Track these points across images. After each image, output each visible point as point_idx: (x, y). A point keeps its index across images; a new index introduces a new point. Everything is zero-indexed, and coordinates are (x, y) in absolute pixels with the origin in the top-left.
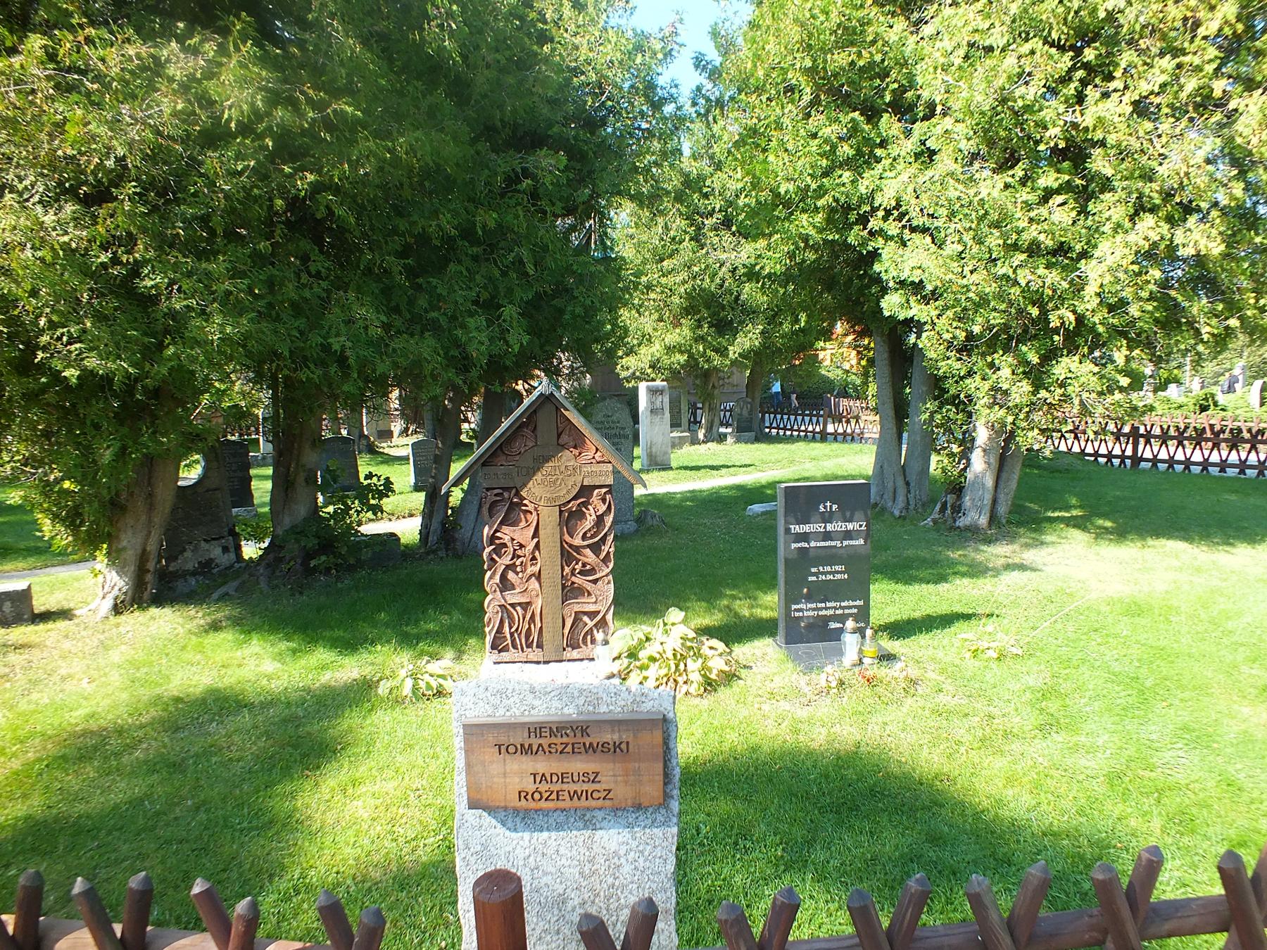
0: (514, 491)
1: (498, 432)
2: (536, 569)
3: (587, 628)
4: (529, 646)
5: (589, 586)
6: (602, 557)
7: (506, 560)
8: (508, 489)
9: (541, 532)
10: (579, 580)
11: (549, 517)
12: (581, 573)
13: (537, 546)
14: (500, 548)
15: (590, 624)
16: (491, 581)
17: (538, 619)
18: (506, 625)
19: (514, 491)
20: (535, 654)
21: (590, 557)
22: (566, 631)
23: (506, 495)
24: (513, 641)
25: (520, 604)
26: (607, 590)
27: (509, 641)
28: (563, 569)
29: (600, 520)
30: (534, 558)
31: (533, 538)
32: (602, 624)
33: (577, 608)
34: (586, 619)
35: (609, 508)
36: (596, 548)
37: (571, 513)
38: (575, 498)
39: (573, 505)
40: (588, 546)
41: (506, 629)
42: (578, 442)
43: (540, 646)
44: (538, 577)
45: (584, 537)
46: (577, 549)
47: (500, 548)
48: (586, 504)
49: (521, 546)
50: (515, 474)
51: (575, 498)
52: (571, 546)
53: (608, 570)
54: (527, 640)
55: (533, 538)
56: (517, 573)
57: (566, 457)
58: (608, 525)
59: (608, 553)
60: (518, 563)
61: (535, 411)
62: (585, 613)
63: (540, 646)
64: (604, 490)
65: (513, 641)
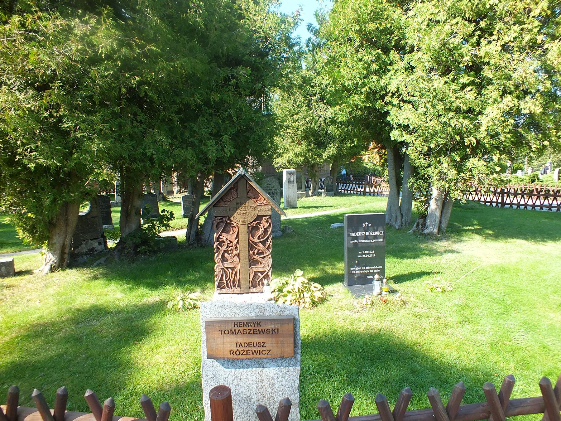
0: (227, 218)
1: (220, 192)
2: (237, 252)
3: (260, 279)
4: (234, 286)
5: (261, 260)
6: (266, 247)
7: (224, 248)
8: (225, 217)
9: (240, 236)
10: (256, 257)
11: (243, 229)
12: (257, 254)
13: (238, 242)
14: (221, 243)
15: (261, 276)
16: (217, 257)
17: (238, 274)
18: (224, 277)
19: (227, 218)
20: (237, 290)
21: (261, 247)
22: (251, 280)
23: (224, 219)
24: (227, 284)
25: (230, 268)
26: (269, 261)
27: (225, 284)
28: (249, 252)
29: (266, 230)
30: (236, 247)
31: (236, 238)
32: (267, 276)
33: (256, 269)
34: (259, 274)
35: (270, 225)
36: (264, 243)
37: (253, 227)
38: (254, 221)
39: (254, 224)
40: (260, 242)
41: (224, 279)
42: (256, 196)
43: (239, 286)
44: (238, 255)
45: (259, 238)
46: (256, 243)
47: (221, 243)
48: (259, 223)
49: (231, 242)
50: (228, 210)
51: (254, 221)
52: (253, 242)
53: (269, 253)
54: (233, 284)
55: (236, 238)
56: (229, 254)
57: (251, 203)
58: (269, 233)
59: (269, 245)
60: (229, 249)
61: (237, 182)
62: (259, 272)
63: (239, 286)
64: (267, 217)
65: (227, 284)
